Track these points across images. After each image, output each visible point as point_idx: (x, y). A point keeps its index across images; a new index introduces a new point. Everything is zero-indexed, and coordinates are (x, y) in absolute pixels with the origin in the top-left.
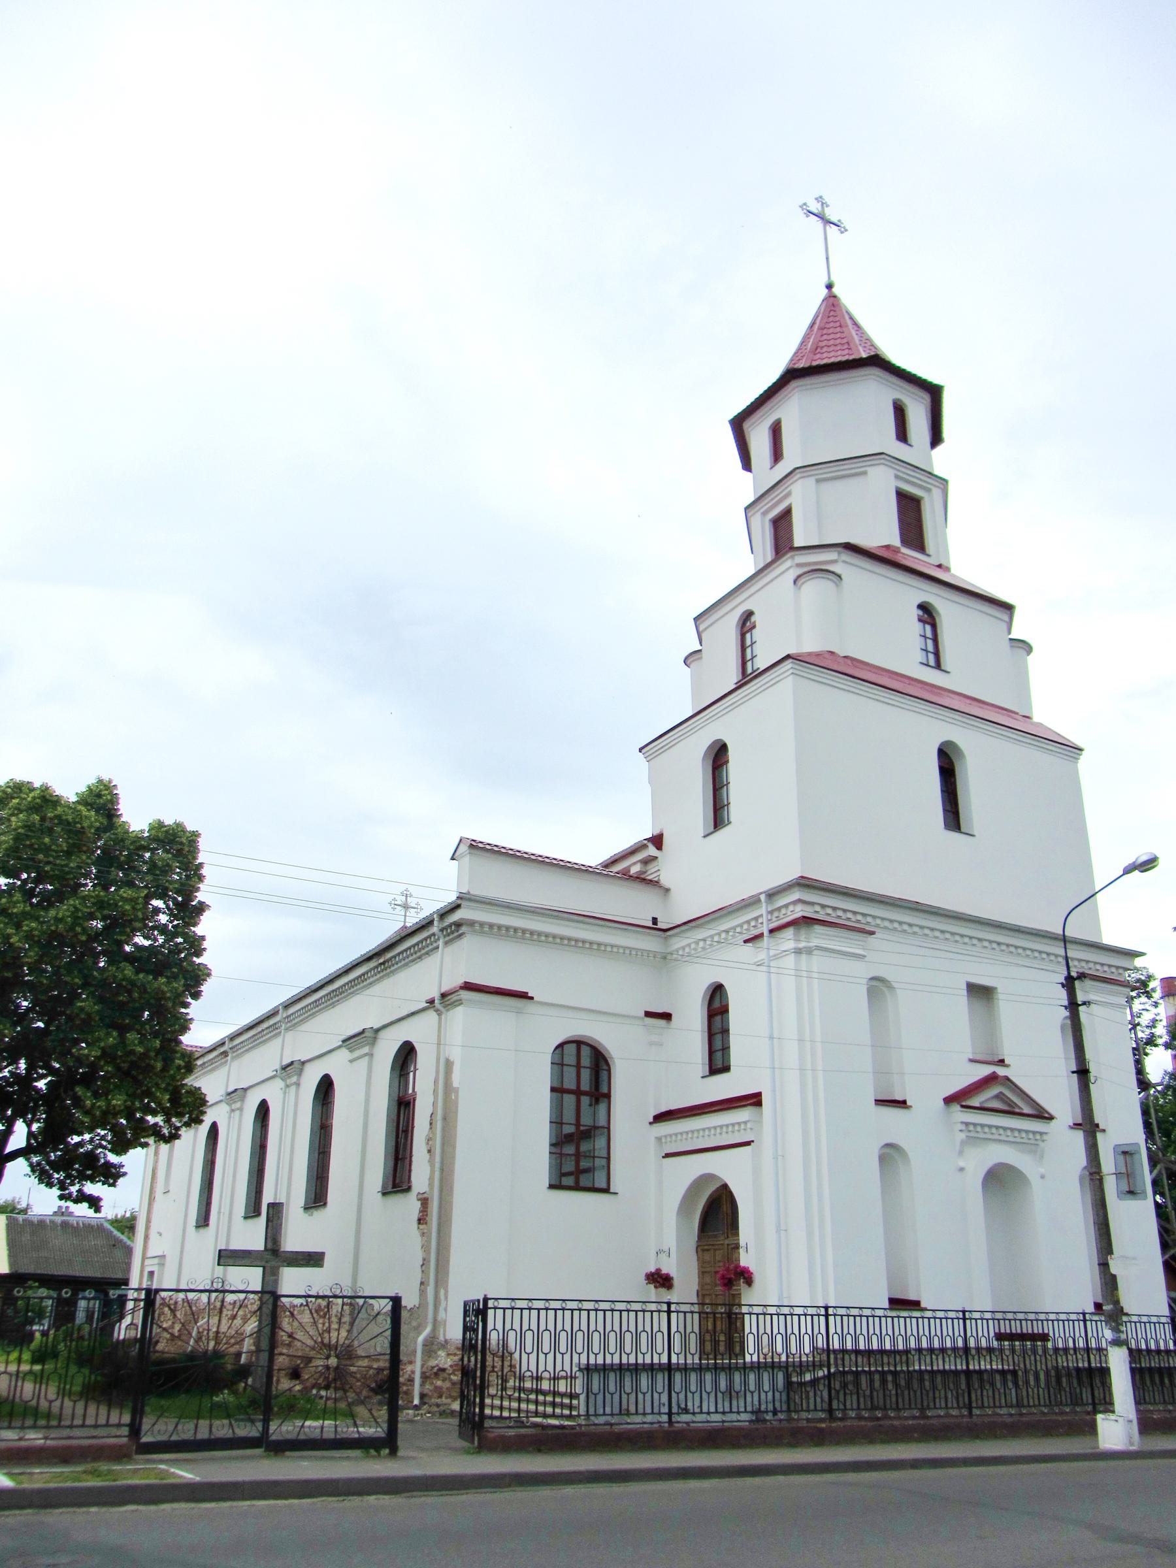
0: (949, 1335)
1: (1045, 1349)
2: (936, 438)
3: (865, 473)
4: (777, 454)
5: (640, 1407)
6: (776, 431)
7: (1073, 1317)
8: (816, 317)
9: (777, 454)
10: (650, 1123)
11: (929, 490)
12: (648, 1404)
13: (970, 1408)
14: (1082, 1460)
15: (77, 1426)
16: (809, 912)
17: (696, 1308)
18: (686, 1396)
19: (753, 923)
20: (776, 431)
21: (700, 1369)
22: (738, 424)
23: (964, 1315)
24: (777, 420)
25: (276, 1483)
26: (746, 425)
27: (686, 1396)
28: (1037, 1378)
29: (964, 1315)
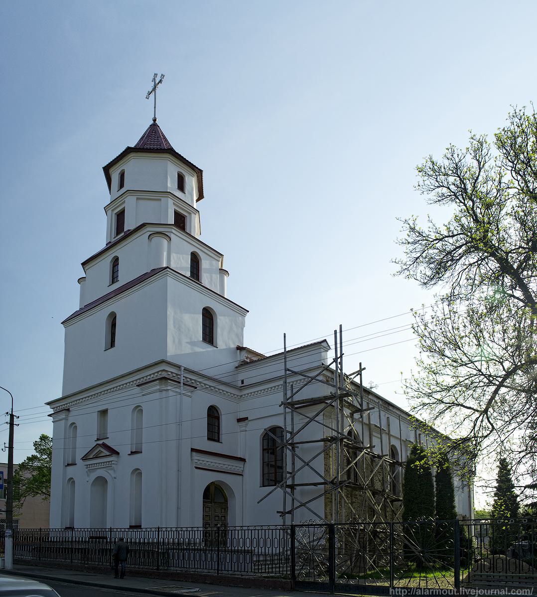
0: (153, 537)
1: (107, 542)
2: (201, 196)
3: (160, 200)
4: (122, 185)
5: (207, 566)
6: (122, 176)
7: (153, 530)
8: (145, 134)
9: (122, 185)
10: (129, 455)
11: (190, 214)
12: (243, 567)
13: (40, 558)
14: (124, 588)
15: (263, 573)
16: (164, 374)
17: (201, 529)
18: (231, 564)
19: (250, 395)
20: (122, 176)
21: (205, 551)
22: (107, 169)
23: (159, 530)
24: (122, 170)
25: (110, 586)
26: (111, 171)
27: (231, 564)
28: (54, 550)
29: (159, 530)
